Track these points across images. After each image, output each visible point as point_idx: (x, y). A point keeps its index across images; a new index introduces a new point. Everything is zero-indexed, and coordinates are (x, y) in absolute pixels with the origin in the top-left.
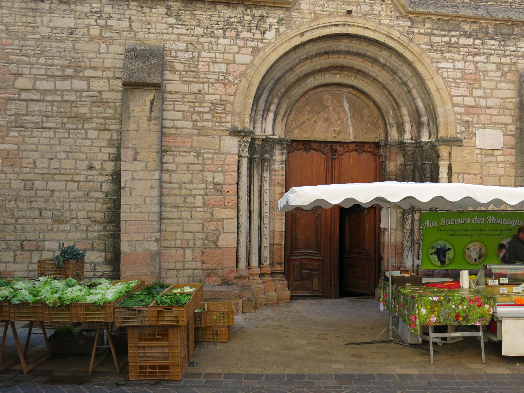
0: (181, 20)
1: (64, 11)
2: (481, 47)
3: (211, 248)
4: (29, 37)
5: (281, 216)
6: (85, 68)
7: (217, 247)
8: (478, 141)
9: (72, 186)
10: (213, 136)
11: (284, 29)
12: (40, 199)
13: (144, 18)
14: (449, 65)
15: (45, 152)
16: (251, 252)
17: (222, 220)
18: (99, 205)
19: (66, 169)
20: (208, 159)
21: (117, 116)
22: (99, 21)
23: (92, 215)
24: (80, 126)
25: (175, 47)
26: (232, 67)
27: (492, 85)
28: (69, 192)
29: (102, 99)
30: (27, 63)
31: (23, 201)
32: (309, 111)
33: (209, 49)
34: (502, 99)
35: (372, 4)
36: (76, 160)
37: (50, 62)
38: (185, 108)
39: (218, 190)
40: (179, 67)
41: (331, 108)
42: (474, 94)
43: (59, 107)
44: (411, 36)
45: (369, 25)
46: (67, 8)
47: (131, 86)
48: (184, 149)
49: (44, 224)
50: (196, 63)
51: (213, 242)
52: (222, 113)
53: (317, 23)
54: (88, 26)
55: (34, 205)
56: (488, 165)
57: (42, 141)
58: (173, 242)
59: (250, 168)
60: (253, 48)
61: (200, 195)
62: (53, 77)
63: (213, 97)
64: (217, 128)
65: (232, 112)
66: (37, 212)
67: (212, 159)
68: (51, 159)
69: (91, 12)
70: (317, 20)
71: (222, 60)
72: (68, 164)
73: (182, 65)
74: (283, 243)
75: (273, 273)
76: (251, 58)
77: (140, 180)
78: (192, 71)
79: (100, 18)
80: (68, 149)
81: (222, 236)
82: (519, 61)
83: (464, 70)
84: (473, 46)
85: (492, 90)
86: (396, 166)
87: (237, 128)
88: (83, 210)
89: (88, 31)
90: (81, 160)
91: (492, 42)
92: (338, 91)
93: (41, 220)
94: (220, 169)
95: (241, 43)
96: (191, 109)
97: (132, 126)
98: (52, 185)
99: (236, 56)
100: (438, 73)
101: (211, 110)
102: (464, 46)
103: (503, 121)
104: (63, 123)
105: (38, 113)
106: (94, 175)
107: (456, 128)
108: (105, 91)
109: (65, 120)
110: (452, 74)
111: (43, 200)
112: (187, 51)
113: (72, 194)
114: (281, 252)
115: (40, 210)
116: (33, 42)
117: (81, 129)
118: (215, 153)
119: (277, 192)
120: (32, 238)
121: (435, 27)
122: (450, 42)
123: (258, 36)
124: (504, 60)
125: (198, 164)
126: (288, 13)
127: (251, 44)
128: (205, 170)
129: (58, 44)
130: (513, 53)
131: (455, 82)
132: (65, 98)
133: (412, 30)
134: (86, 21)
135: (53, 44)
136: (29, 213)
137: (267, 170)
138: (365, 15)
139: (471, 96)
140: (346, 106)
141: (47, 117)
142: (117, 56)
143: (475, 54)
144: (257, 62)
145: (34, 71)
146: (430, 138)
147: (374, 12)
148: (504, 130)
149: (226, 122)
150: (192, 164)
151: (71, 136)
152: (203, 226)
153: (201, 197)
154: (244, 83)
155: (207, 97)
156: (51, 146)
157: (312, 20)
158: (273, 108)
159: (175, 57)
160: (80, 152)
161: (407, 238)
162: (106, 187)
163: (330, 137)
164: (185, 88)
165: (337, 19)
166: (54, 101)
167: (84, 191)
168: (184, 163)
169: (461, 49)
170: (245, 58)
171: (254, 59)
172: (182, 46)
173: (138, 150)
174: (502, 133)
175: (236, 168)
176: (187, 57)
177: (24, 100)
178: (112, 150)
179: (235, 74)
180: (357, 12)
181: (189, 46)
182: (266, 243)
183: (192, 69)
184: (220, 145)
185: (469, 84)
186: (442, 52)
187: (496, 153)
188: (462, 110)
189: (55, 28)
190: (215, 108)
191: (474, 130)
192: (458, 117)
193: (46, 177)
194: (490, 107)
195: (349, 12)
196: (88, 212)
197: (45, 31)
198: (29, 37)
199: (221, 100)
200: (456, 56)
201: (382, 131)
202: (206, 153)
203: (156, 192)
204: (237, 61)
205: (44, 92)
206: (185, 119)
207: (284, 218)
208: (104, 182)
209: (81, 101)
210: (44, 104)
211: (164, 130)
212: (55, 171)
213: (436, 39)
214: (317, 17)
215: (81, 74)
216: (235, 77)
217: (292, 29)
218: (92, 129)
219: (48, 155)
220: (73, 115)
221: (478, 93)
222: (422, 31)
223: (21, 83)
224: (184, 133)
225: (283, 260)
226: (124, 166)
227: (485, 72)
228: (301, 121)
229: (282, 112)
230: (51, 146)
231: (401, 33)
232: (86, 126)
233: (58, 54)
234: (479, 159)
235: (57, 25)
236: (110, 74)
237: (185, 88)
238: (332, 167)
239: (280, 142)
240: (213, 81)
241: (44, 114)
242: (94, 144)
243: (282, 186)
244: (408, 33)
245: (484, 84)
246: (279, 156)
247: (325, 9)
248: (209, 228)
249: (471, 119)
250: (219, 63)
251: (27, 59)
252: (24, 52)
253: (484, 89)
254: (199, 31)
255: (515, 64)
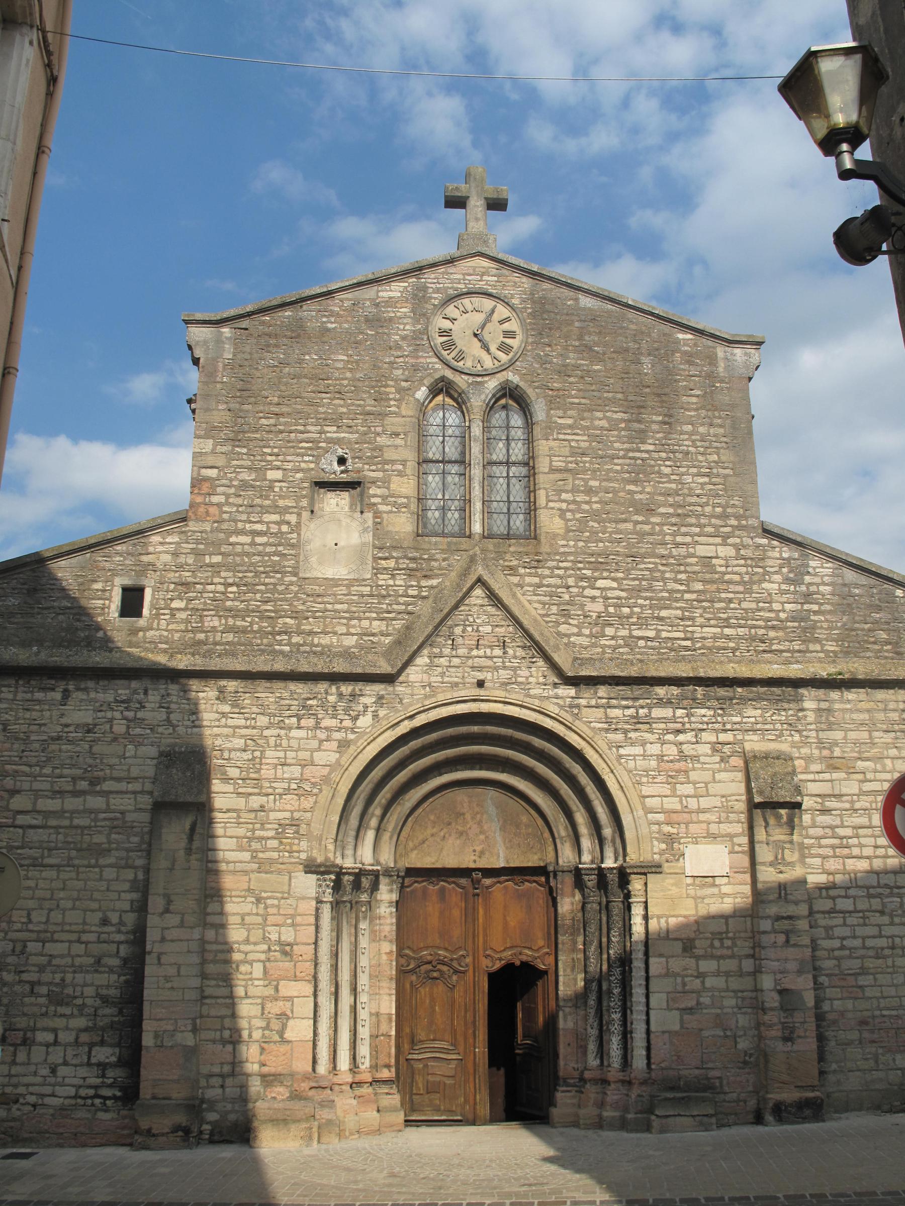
0: (237, 706)
1: (81, 701)
2: (686, 719)
3: (275, 1042)
4: (32, 738)
5: (390, 989)
6: (105, 779)
7: (284, 1041)
8: (687, 865)
9: (79, 949)
10: (279, 872)
11: (385, 712)
12: (33, 969)
13: (187, 707)
14: (638, 750)
15: (44, 899)
16: (339, 1048)
17: (290, 999)
18: (114, 977)
19: (70, 924)
20: (273, 906)
21: (144, 846)
22: (126, 713)
23: (104, 992)
24: (93, 861)
25: (229, 745)
26: (308, 771)
27: (707, 776)
28: (73, 957)
29: (125, 822)
30: (27, 775)
31: (9, 972)
32: (434, 822)
33: (276, 746)
34: (723, 796)
35: (516, 668)
36: (85, 911)
37: (58, 771)
38: (241, 832)
39: (285, 953)
40: (233, 772)
41: (468, 816)
42: (679, 793)
43: (66, 835)
44: (576, 711)
45: (513, 697)
46: (85, 697)
47: (162, 808)
48: (238, 893)
49: (36, 1005)
50: (258, 766)
51: (278, 1032)
52: (294, 838)
53: (434, 700)
54: (111, 721)
55: (25, 977)
56: (706, 901)
57: (41, 884)
58: (218, 1033)
59: (337, 919)
60: (339, 741)
61: (259, 961)
62: (61, 793)
63: (280, 815)
64: (285, 860)
65: (308, 836)
66: (27, 987)
67: (278, 907)
68: (51, 910)
69: (116, 701)
70: (434, 696)
71: (294, 761)
72: (74, 917)
73: (238, 770)
74: (393, 1033)
75: (375, 1082)
76: (337, 755)
77: (172, 941)
78: (252, 779)
79: (127, 709)
80: (75, 894)
81: (291, 1023)
82: (747, 738)
83: (660, 758)
84: (674, 719)
85: (706, 784)
86: (572, 904)
87: (315, 859)
88: (92, 985)
89: (111, 728)
90: (93, 911)
91: (703, 711)
92: (479, 790)
93: (33, 999)
94: (289, 921)
95: (322, 735)
96: (249, 834)
97: (164, 864)
98: (50, 948)
99: (315, 754)
100: (620, 764)
101: (278, 833)
102: (660, 720)
103: (729, 831)
104: (70, 858)
105: (37, 845)
106: (108, 933)
107: (653, 846)
108: (129, 811)
109: (74, 853)
110: (640, 763)
111: (36, 969)
112: (245, 751)
113: (78, 961)
114: (390, 1048)
115: (33, 984)
116: (36, 746)
117: (93, 867)
118: (283, 898)
119: (383, 951)
120: (18, 1026)
121: (612, 695)
122: (637, 716)
123: (348, 723)
124: (723, 737)
125: (257, 914)
126: (390, 689)
127: (337, 735)
128: (268, 923)
129: (69, 747)
130: (735, 726)
131: (647, 776)
132: (76, 822)
133: (577, 701)
134: (109, 714)
135: (64, 747)
136: (18, 988)
137: (365, 918)
138: (504, 685)
139: (674, 795)
140: (492, 810)
141: (50, 850)
142: (149, 761)
143: (678, 732)
144: (344, 761)
145: (36, 785)
146: (616, 860)
147: (520, 679)
148: (729, 844)
149: (299, 852)
150: (249, 914)
151: (81, 876)
152: (263, 1008)
153: (260, 965)
154: (327, 792)
155: (272, 816)
156: (52, 891)
157: (426, 697)
158: (374, 822)
159: (229, 759)
160: (91, 899)
161: (591, 1020)
162: (124, 950)
163: (468, 861)
164: (240, 803)
165: (463, 693)
166: (61, 827)
167: (93, 956)
168: (238, 914)
169: (654, 725)
170: (328, 756)
171: (341, 757)
172: (239, 743)
173: (172, 897)
174: (727, 850)
175: (312, 920)
176: (246, 758)
177: (21, 827)
178: (135, 896)
179: (313, 780)
180: (492, 681)
181: (249, 742)
182: (364, 1032)
183: (253, 776)
184: (290, 885)
185: (671, 776)
186: (626, 732)
187: (718, 881)
188: (661, 817)
189: (67, 726)
190: (284, 831)
191: (681, 846)
192: (655, 828)
193: (42, 935)
194: (704, 811)
195: (481, 684)
196: (98, 987)
197: (54, 729)
198: (32, 738)
199: (292, 819)
200: (647, 736)
201: (551, 848)
202: (269, 898)
203: (195, 959)
204: (317, 761)
205: (47, 814)
206: (241, 849)
207: (394, 992)
208: (122, 942)
209: (96, 826)
210: (48, 831)
211: (210, 865)
212: (55, 928)
213: (615, 713)
214: (434, 693)
215: (98, 788)
216: (314, 784)
217: (398, 711)
218: (110, 866)
219: (47, 904)
220: (85, 846)
221: (688, 789)
222: (593, 702)
223: (17, 803)
224: (238, 869)
225: (393, 1061)
226: (153, 921)
227: (695, 758)
228: (421, 837)
229: (391, 827)
230: (52, 891)
231: (561, 707)
232: (102, 861)
233: (68, 761)
234: (692, 892)
235: (69, 722)
236: (137, 786)
237: (240, 803)
238: (474, 908)
239: (387, 873)
240: (281, 791)
241: (45, 845)
242: (111, 888)
243: (391, 941)
244: (571, 706)
245: (693, 776)
246: (387, 894)
247: (446, 679)
248: (272, 1011)
249: (675, 831)
250: (290, 765)
251: (26, 769)
252: (25, 759)
253: (694, 783)
254: (263, 720)
255: (741, 742)
